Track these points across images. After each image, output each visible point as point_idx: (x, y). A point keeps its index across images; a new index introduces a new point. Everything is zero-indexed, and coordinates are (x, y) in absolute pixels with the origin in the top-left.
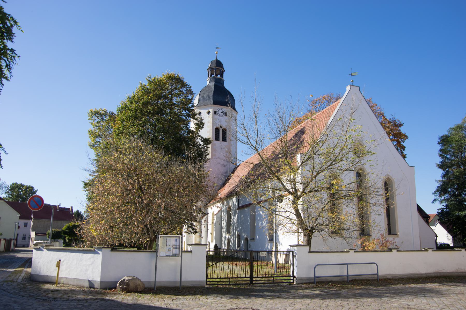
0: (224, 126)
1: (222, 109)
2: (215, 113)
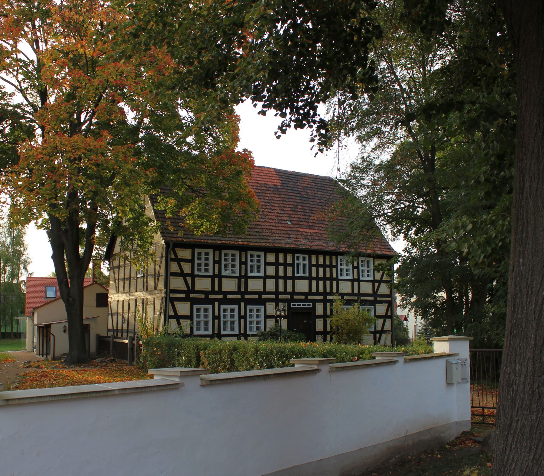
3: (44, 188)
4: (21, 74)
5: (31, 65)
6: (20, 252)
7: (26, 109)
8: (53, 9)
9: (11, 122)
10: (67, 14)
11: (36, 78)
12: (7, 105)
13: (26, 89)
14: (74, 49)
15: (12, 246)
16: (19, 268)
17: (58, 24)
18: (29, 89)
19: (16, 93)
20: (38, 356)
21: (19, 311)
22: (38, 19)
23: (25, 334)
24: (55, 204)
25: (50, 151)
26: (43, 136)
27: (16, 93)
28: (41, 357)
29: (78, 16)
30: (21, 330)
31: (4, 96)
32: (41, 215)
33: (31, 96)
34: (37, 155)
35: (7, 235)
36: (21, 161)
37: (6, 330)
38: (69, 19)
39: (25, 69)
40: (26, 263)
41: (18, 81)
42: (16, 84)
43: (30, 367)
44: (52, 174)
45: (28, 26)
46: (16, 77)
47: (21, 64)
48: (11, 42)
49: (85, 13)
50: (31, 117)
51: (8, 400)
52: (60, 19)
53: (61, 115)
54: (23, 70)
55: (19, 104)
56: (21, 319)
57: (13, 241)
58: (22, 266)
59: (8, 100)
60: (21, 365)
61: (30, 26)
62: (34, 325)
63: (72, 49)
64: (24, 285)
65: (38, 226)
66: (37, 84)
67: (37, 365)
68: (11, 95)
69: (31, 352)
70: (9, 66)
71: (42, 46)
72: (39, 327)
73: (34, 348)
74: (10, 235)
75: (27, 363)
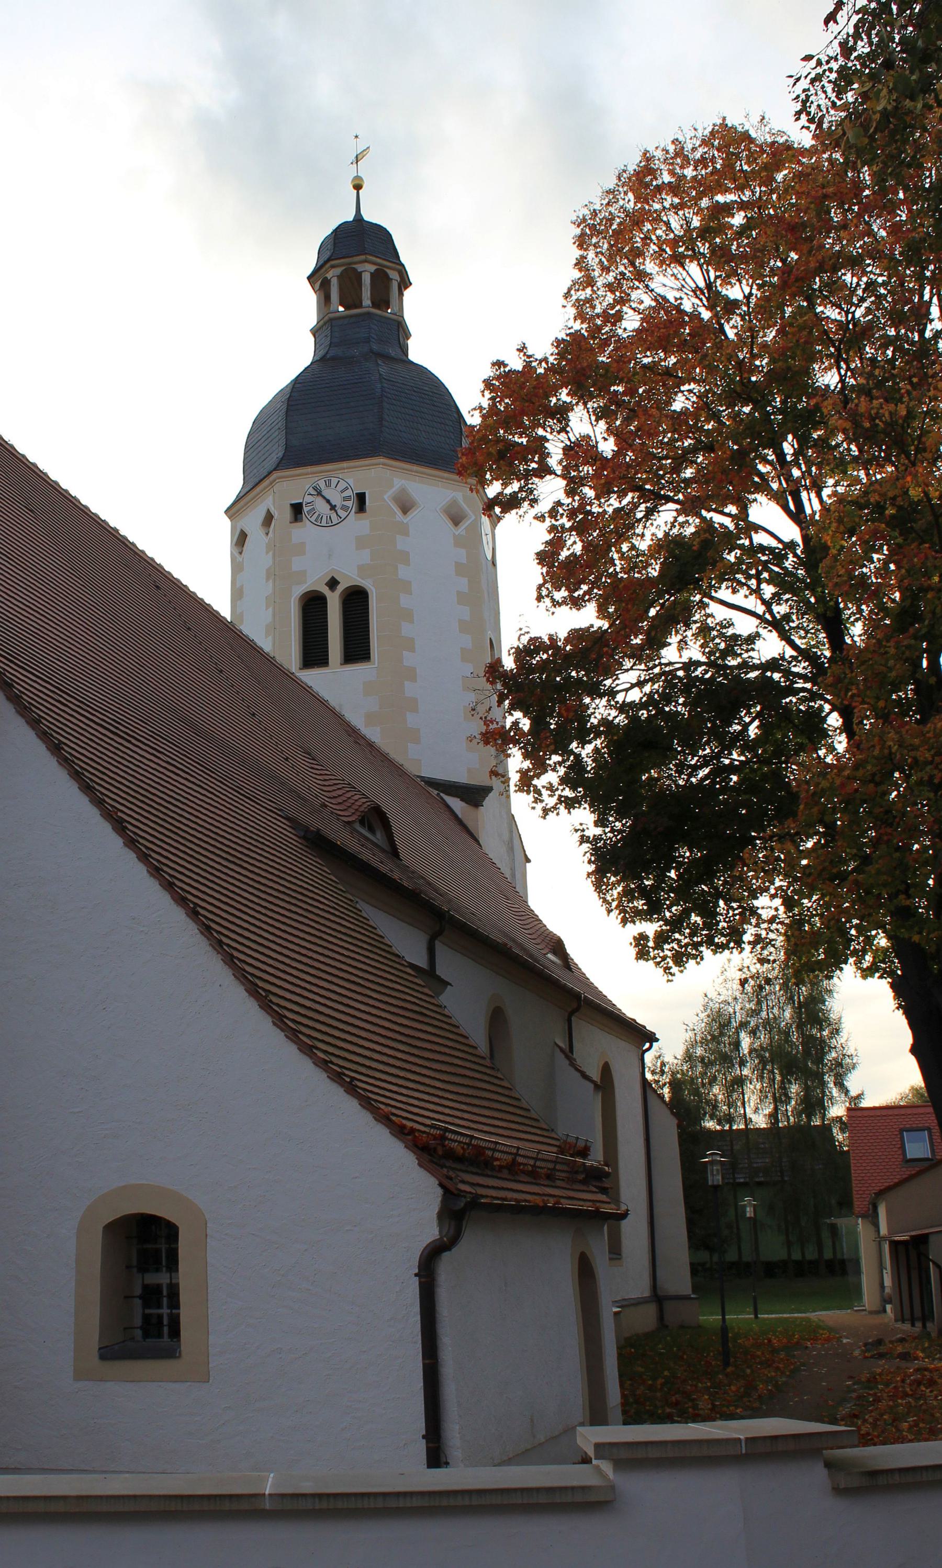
0: (350, 577)
2: (297, 509)
3: (872, 869)
4: (768, 582)
5: (790, 556)
6: (822, 1041)
7: (794, 670)
8: (825, 403)
9: (758, 708)
10: (862, 409)
11: (808, 587)
12: (745, 666)
13: (787, 617)
14: (897, 492)
15: (797, 1027)
16: (823, 1084)
17: (840, 437)
18: (794, 617)
19: (763, 632)
20: (899, 1325)
21: (833, 1202)
22: (790, 437)
23: (857, 1262)
24: (907, 908)
25: (875, 769)
26: (848, 728)
27: (763, 632)
28: (907, 1326)
29: (892, 407)
30: (846, 1254)
31: (733, 647)
32: (869, 940)
33: (802, 633)
34: (843, 785)
35: (782, 999)
36: (801, 807)
37: (803, 1254)
38: (872, 419)
39: (776, 569)
40: (841, 1070)
41: (764, 602)
42: (760, 609)
43: (881, 1356)
44: (889, 830)
45: (765, 460)
46: (757, 592)
47: (764, 558)
48: (732, 509)
49: (908, 392)
50: (808, 685)
51: (874, 1474)
52: (848, 425)
53: (891, 669)
54: (770, 571)
55: (773, 659)
56: (842, 1223)
57: (800, 1013)
58: (829, 1079)
59: (745, 655)
60: (857, 1353)
61: (772, 457)
62: (880, 1240)
63: (890, 494)
64: (842, 1130)
65: (863, 970)
66: (812, 600)
67: (900, 1349)
68: (752, 639)
69: (877, 1312)
70: (733, 569)
71: (811, 504)
72: (895, 1245)
73: (886, 1300)
74: (791, 998)
75: (872, 1344)
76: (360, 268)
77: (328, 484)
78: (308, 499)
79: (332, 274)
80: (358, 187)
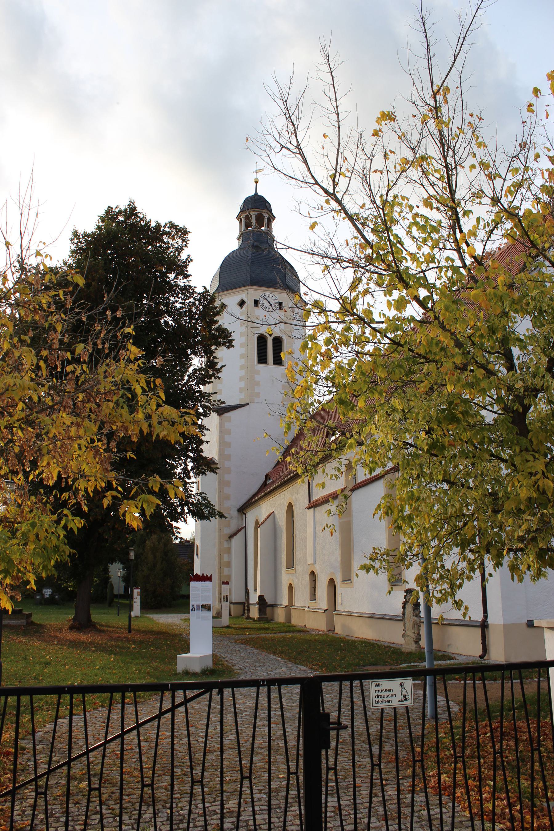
1: (271, 295)
2: (256, 303)
76: (265, 215)
77: (269, 296)
78: (261, 299)
79: (243, 216)
80: (256, 182)
